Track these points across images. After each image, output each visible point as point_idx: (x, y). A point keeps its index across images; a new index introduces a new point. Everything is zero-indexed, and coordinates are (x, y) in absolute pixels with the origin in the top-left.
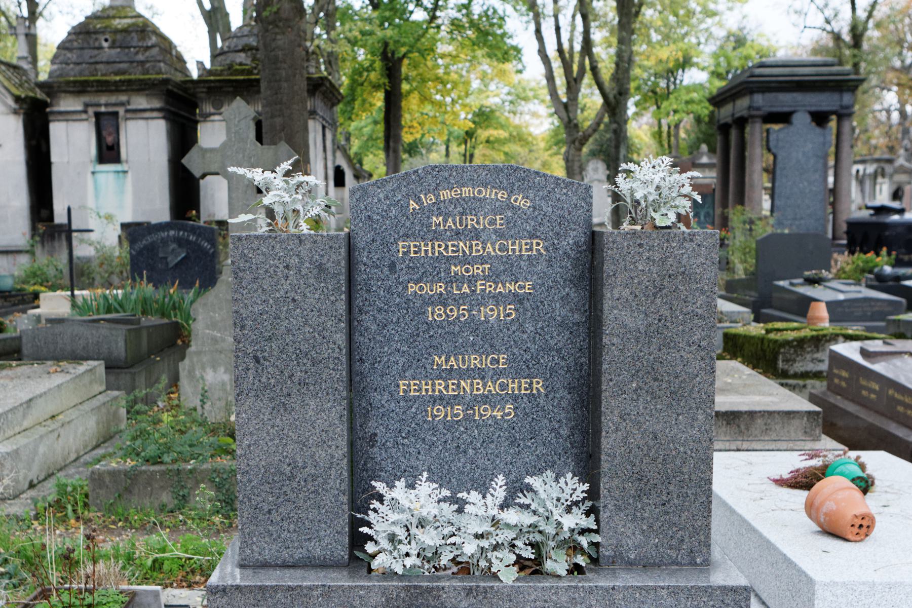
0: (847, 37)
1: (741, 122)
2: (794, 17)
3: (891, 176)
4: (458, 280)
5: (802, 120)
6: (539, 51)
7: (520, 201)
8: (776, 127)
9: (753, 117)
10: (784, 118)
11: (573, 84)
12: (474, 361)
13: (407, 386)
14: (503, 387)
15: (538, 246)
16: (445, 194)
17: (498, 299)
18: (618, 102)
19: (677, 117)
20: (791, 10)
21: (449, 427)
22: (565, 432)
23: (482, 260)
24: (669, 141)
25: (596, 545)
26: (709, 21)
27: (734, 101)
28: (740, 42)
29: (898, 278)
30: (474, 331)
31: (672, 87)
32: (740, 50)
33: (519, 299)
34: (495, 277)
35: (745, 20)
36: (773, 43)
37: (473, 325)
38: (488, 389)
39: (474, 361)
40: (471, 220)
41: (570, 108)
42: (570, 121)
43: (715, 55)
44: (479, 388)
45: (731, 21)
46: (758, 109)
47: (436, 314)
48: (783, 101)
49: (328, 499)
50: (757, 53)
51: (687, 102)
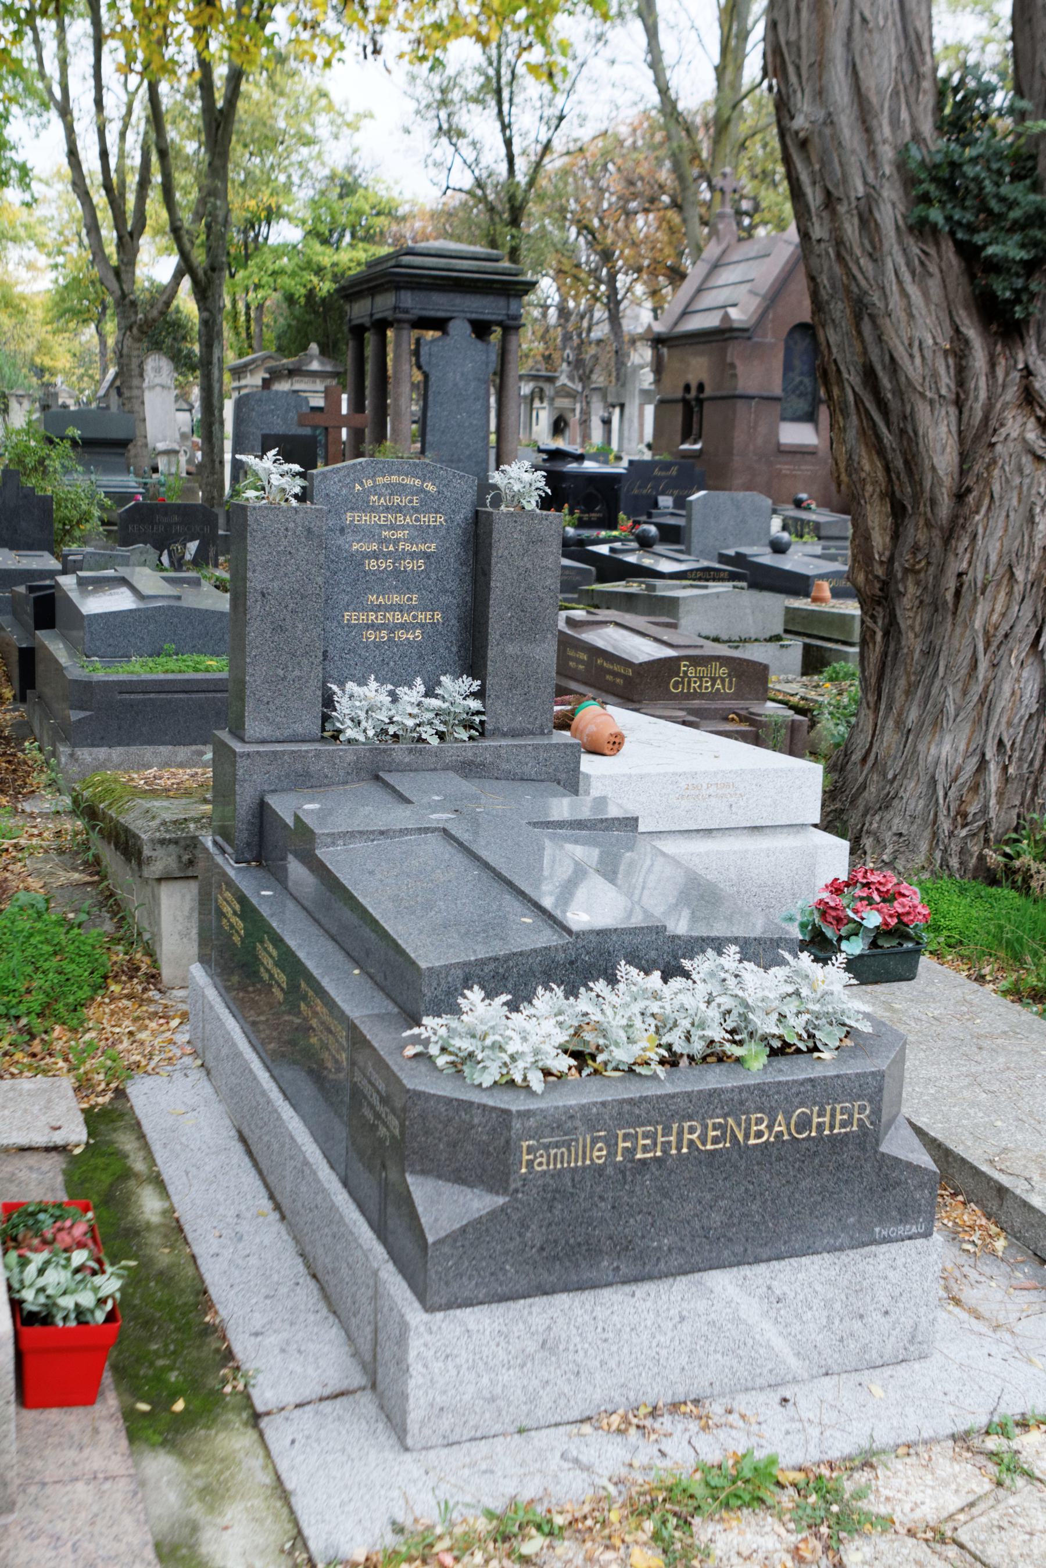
0: (502, 207)
1: (381, 326)
2: (432, 172)
3: (552, 400)
4: (386, 541)
5: (460, 329)
6: (74, 184)
7: (430, 487)
8: (430, 334)
9: (399, 321)
10: (440, 324)
11: (128, 243)
12: (396, 599)
13: (350, 616)
14: (415, 617)
15: (441, 519)
16: (380, 480)
17: (413, 555)
18: (210, 282)
19: (261, 294)
20: (430, 161)
21: (378, 645)
22: (454, 649)
23: (403, 527)
24: (248, 328)
25: (482, 722)
26: (305, 151)
27: (373, 296)
28: (348, 189)
29: (581, 543)
30: (397, 578)
31: (251, 246)
32: (347, 200)
33: (427, 556)
34: (411, 540)
35: (356, 157)
36: (395, 194)
37: (396, 573)
38: (409, 617)
39: (396, 599)
40: (397, 500)
41: (123, 276)
42: (124, 296)
43: (314, 203)
44: (398, 618)
45: (335, 155)
46: (406, 311)
47: (371, 565)
48: (438, 304)
49: (308, 693)
50: (373, 208)
51: (274, 273)
